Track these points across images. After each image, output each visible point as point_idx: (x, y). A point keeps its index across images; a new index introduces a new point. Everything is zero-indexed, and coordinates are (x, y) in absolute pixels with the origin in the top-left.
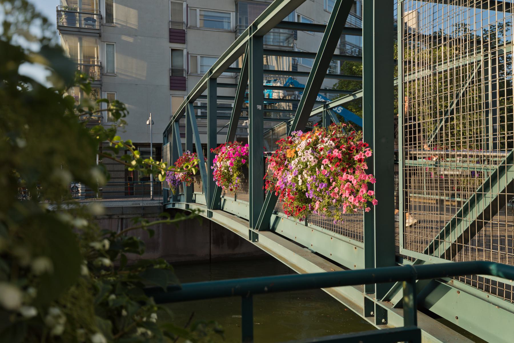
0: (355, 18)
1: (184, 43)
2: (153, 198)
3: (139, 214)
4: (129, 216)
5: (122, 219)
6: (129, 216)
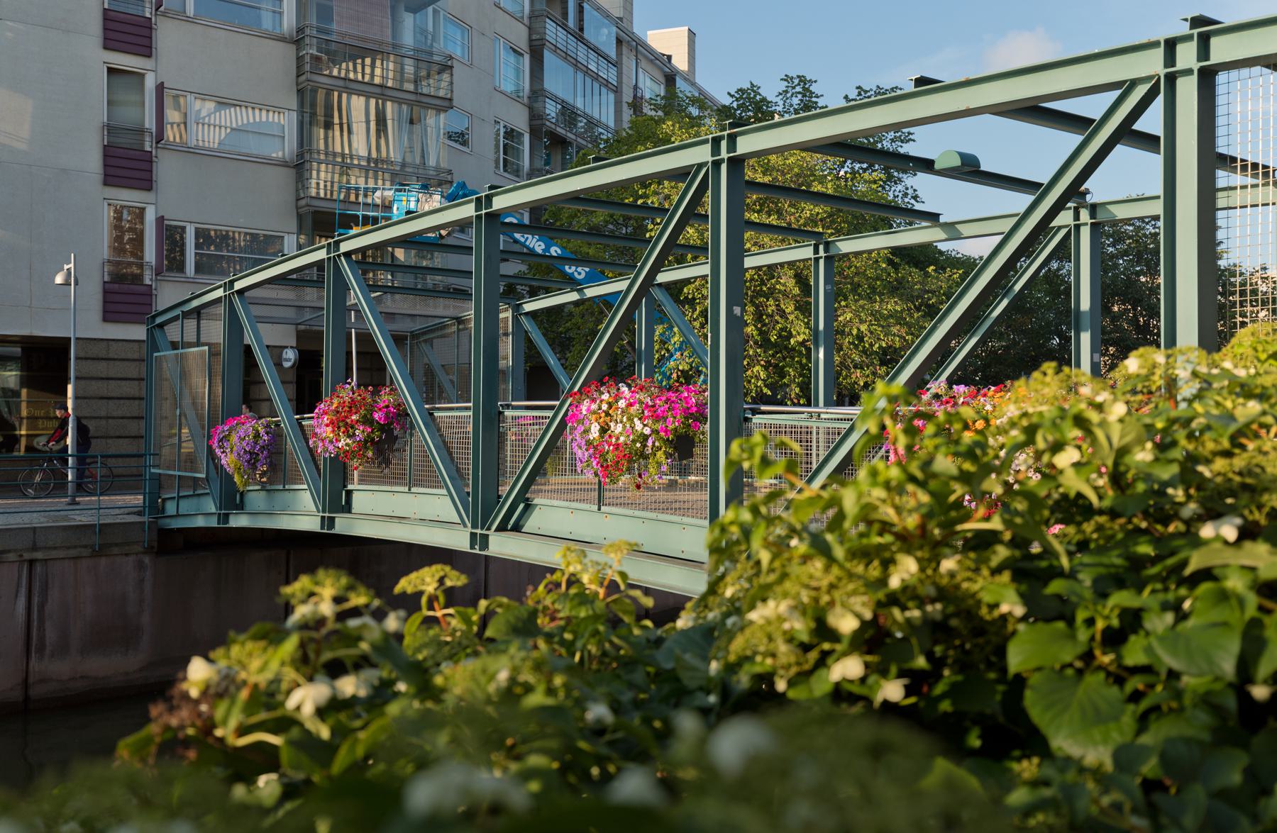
0: (565, 33)
1: (149, 56)
3: (85, 547)
4: (54, 554)
5: (32, 562)
6: (54, 554)
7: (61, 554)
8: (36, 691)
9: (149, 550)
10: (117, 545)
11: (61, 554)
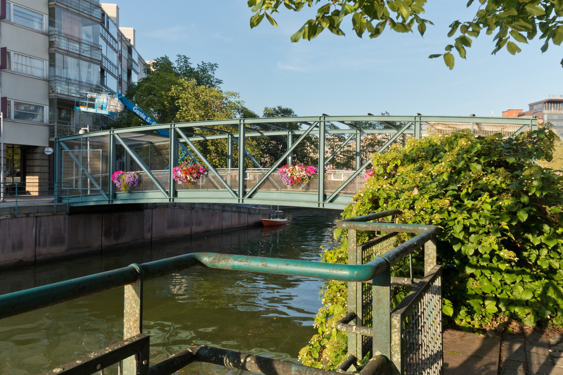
2: (3, 199)
3: (51, 212)
5: (37, 217)
7: (45, 214)
8: (38, 258)
9: (67, 214)
10: (59, 212)
11: (45, 214)
